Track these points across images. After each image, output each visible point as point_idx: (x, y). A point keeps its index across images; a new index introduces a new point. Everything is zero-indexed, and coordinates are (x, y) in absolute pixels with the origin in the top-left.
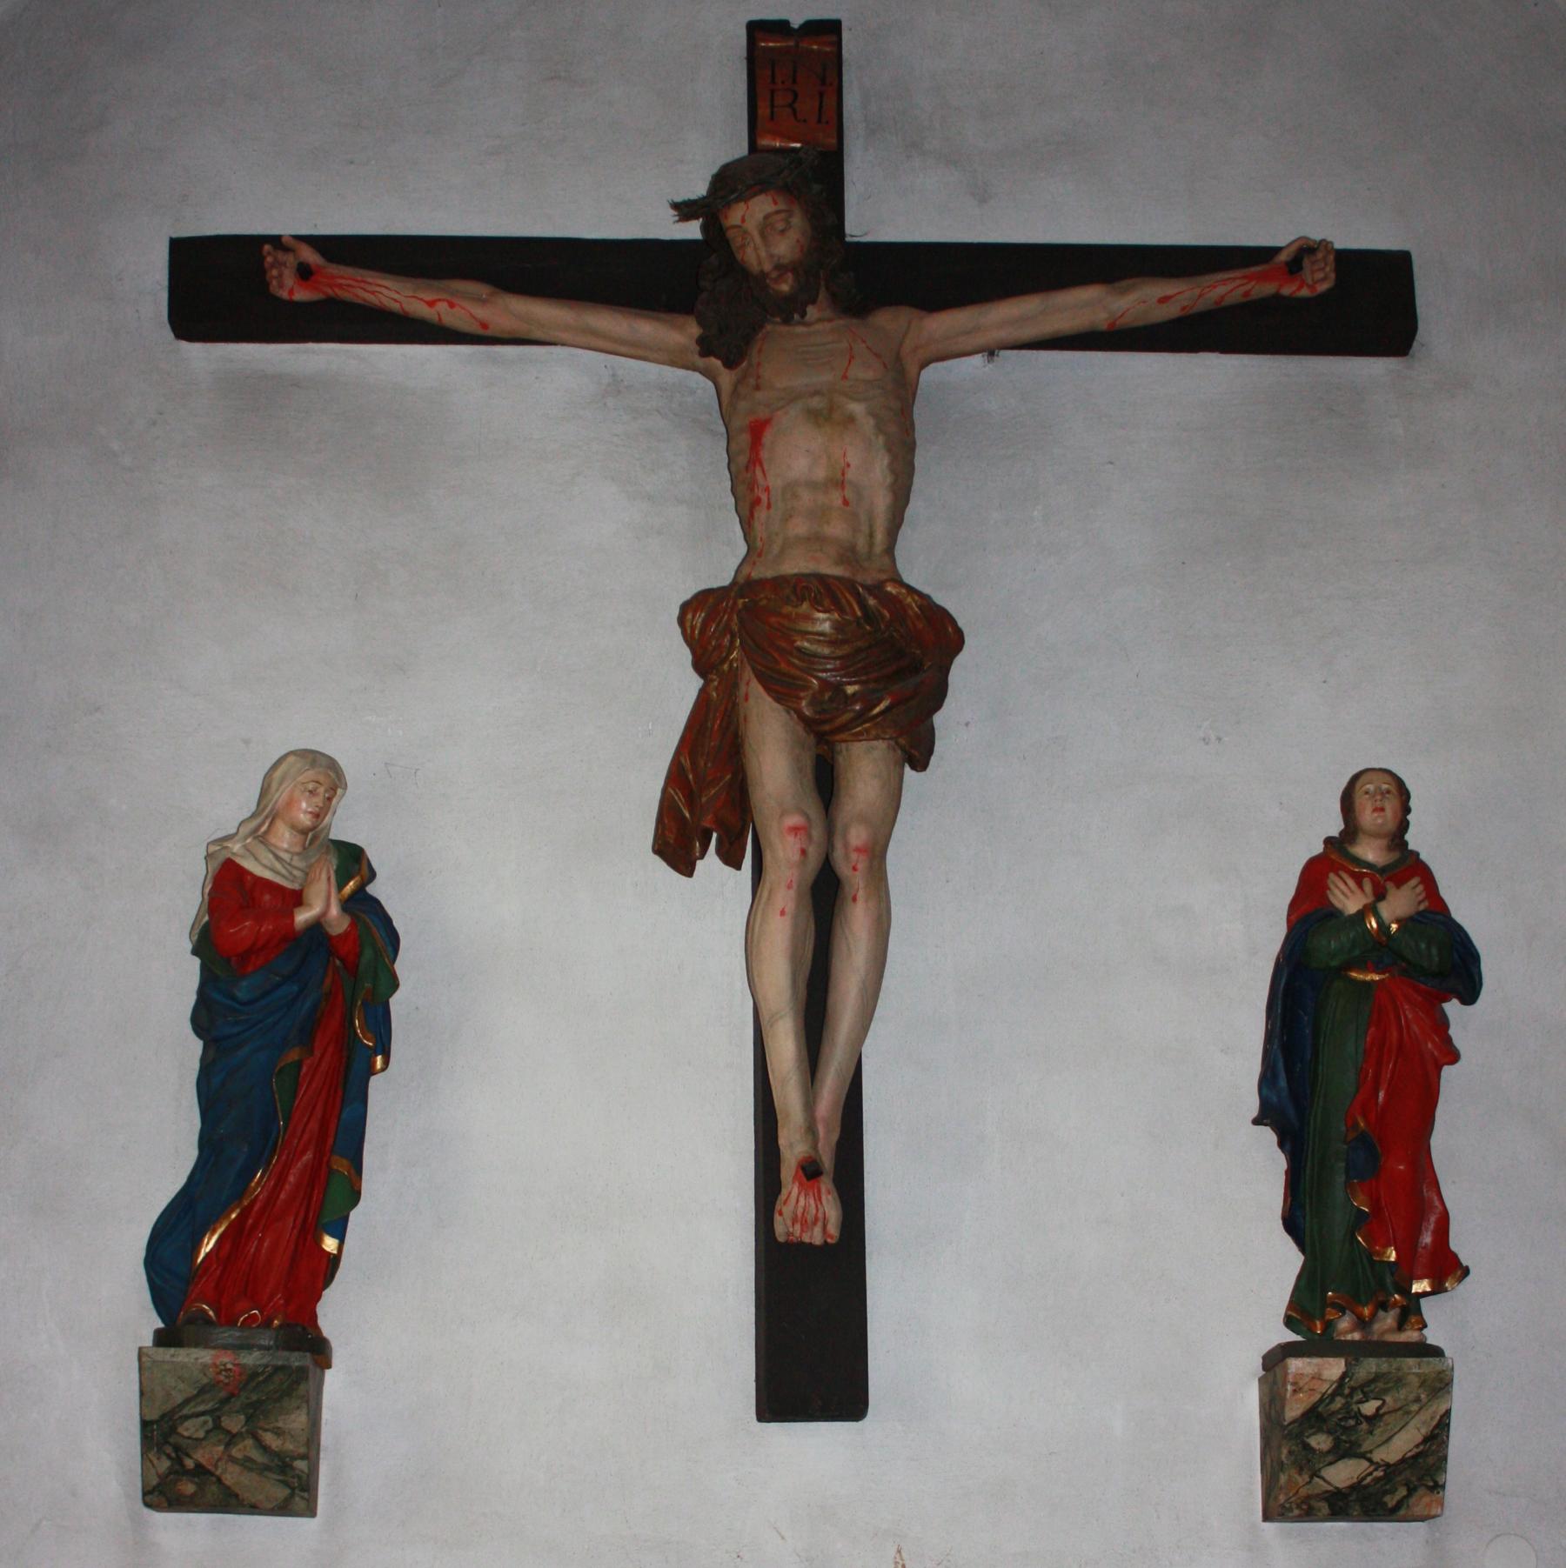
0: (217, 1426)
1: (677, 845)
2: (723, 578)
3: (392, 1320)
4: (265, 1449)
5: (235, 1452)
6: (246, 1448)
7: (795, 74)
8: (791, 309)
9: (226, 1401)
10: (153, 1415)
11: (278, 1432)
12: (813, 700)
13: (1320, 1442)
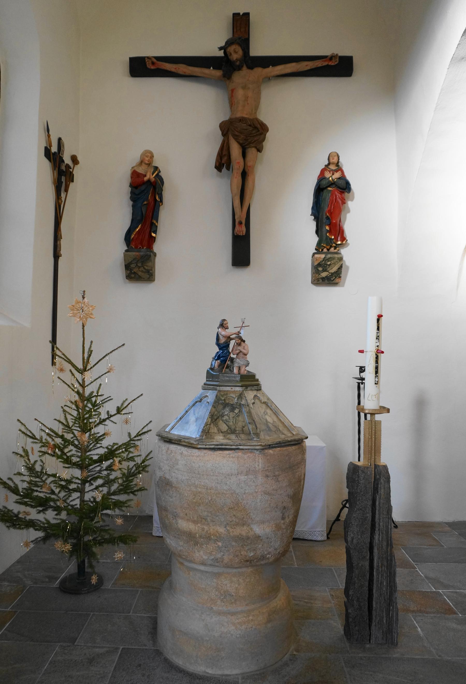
0: (137, 265)
1: (219, 167)
2: (227, 118)
3: (167, 247)
4: (145, 269)
5: (140, 270)
6: (142, 269)
7: (241, 22)
8: (239, 68)
9: (138, 261)
10: (126, 264)
11: (147, 266)
12: (241, 142)
13: (320, 269)
